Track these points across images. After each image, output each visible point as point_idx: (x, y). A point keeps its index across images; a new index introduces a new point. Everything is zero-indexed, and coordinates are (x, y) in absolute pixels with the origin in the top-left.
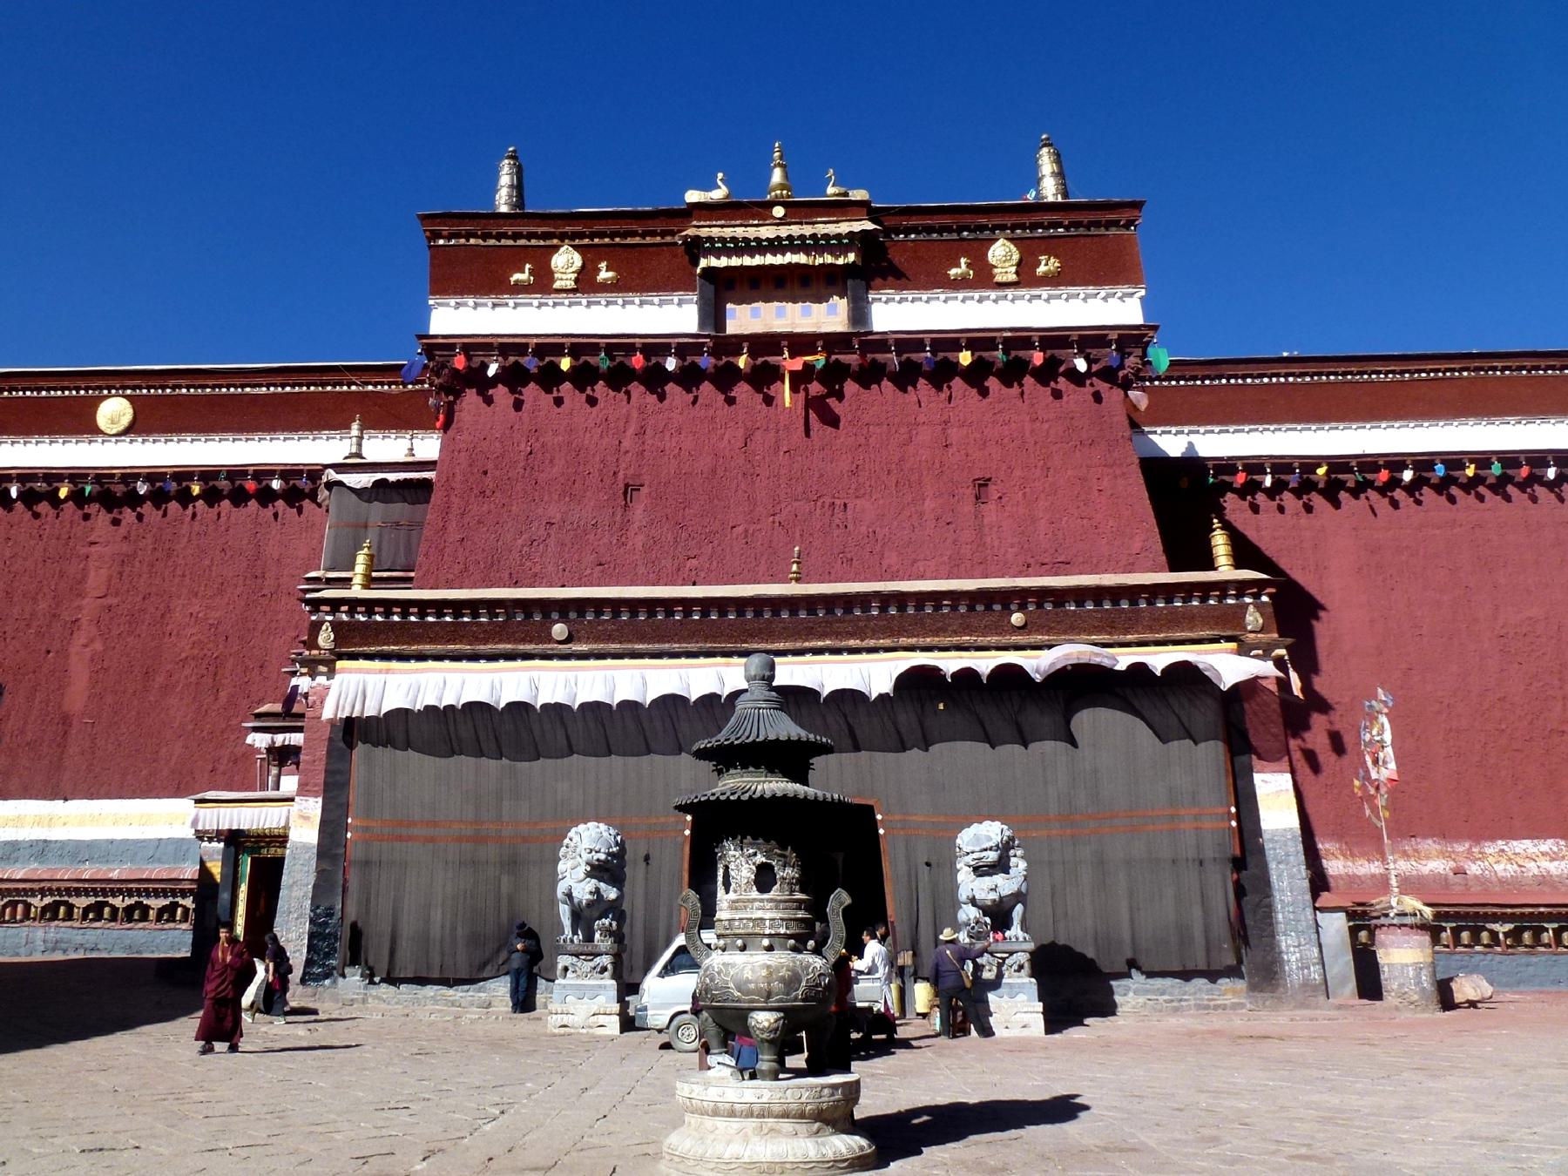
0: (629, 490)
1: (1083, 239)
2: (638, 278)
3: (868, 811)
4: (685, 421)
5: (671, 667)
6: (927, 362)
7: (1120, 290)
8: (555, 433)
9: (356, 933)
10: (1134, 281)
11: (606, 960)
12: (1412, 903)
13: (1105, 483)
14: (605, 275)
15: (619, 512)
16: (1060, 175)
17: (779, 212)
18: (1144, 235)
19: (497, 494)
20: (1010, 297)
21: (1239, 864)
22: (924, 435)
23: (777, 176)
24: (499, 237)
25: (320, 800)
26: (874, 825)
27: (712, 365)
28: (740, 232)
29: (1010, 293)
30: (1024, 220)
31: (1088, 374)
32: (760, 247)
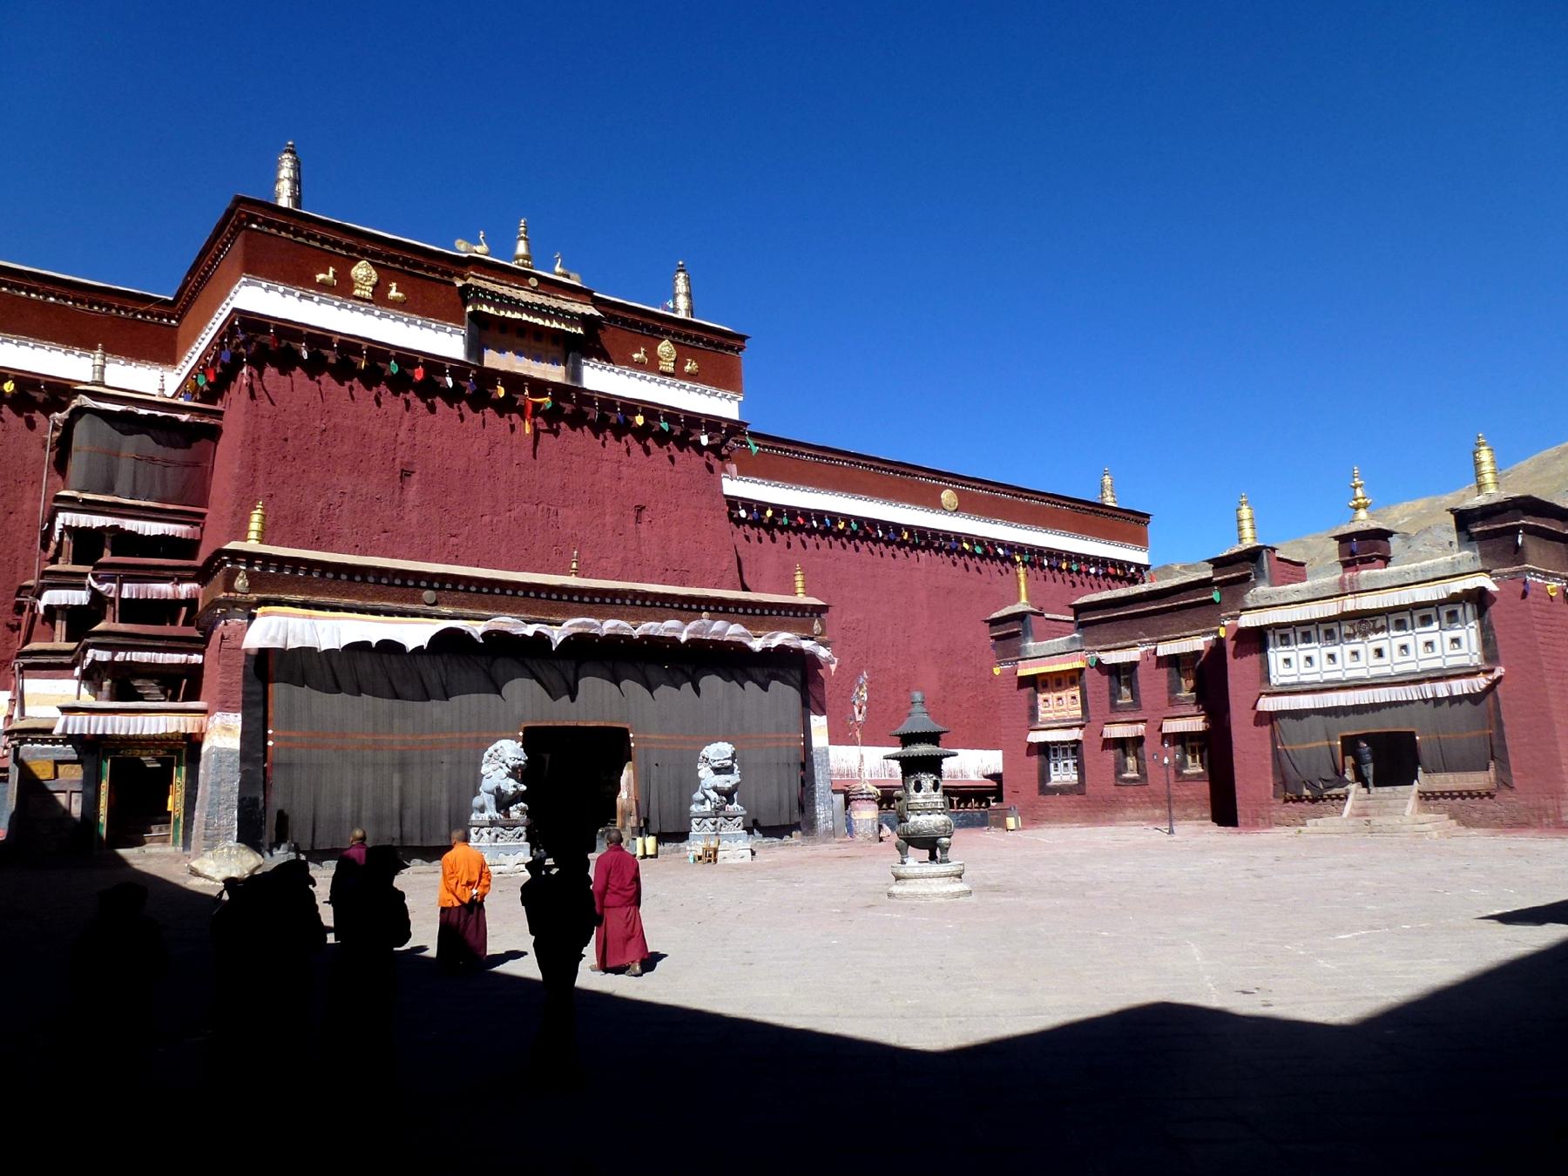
0: (406, 474)
1: (711, 351)
2: (419, 306)
3: (625, 732)
4: (448, 431)
5: (304, 617)
6: (613, 417)
8: (345, 417)
9: (282, 818)
10: (738, 390)
11: (522, 829)
12: (873, 789)
13: (709, 522)
15: (397, 491)
16: (296, 182)
17: (533, 282)
18: (747, 359)
19: (298, 460)
20: (316, 299)
21: (803, 766)
22: (606, 468)
23: (521, 248)
24: (308, 237)
25: (240, 716)
26: (628, 740)
27: (471, 387)
28: (505, 290)
29: (668, 380)
30: (654, 327)
31: (708, 447)
32: (515, 305)
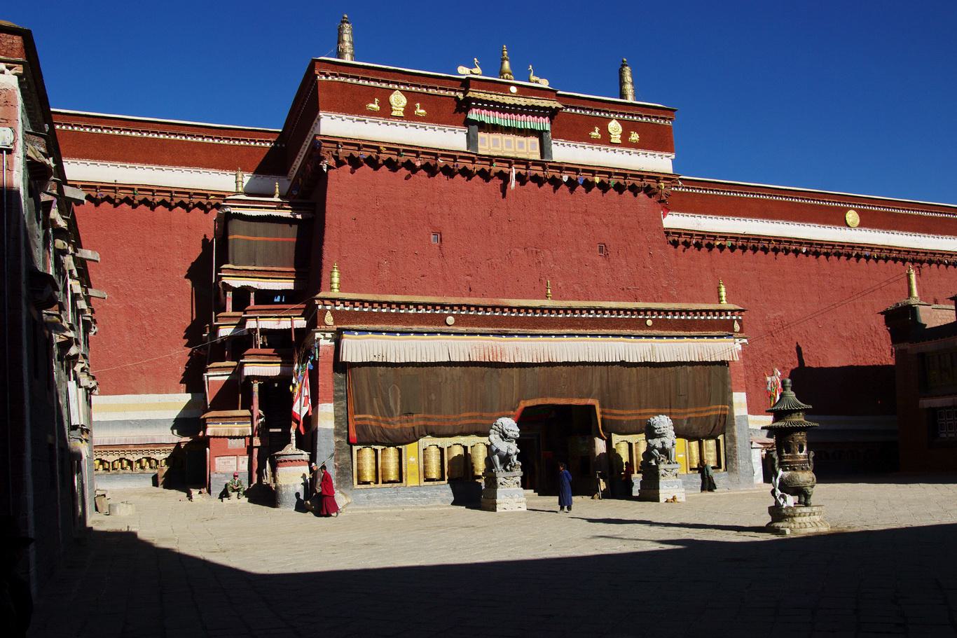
7: (665, 154)
10: (671, 152)
14: (420, 111)
17: (513, 89)
29: (617, 149)
